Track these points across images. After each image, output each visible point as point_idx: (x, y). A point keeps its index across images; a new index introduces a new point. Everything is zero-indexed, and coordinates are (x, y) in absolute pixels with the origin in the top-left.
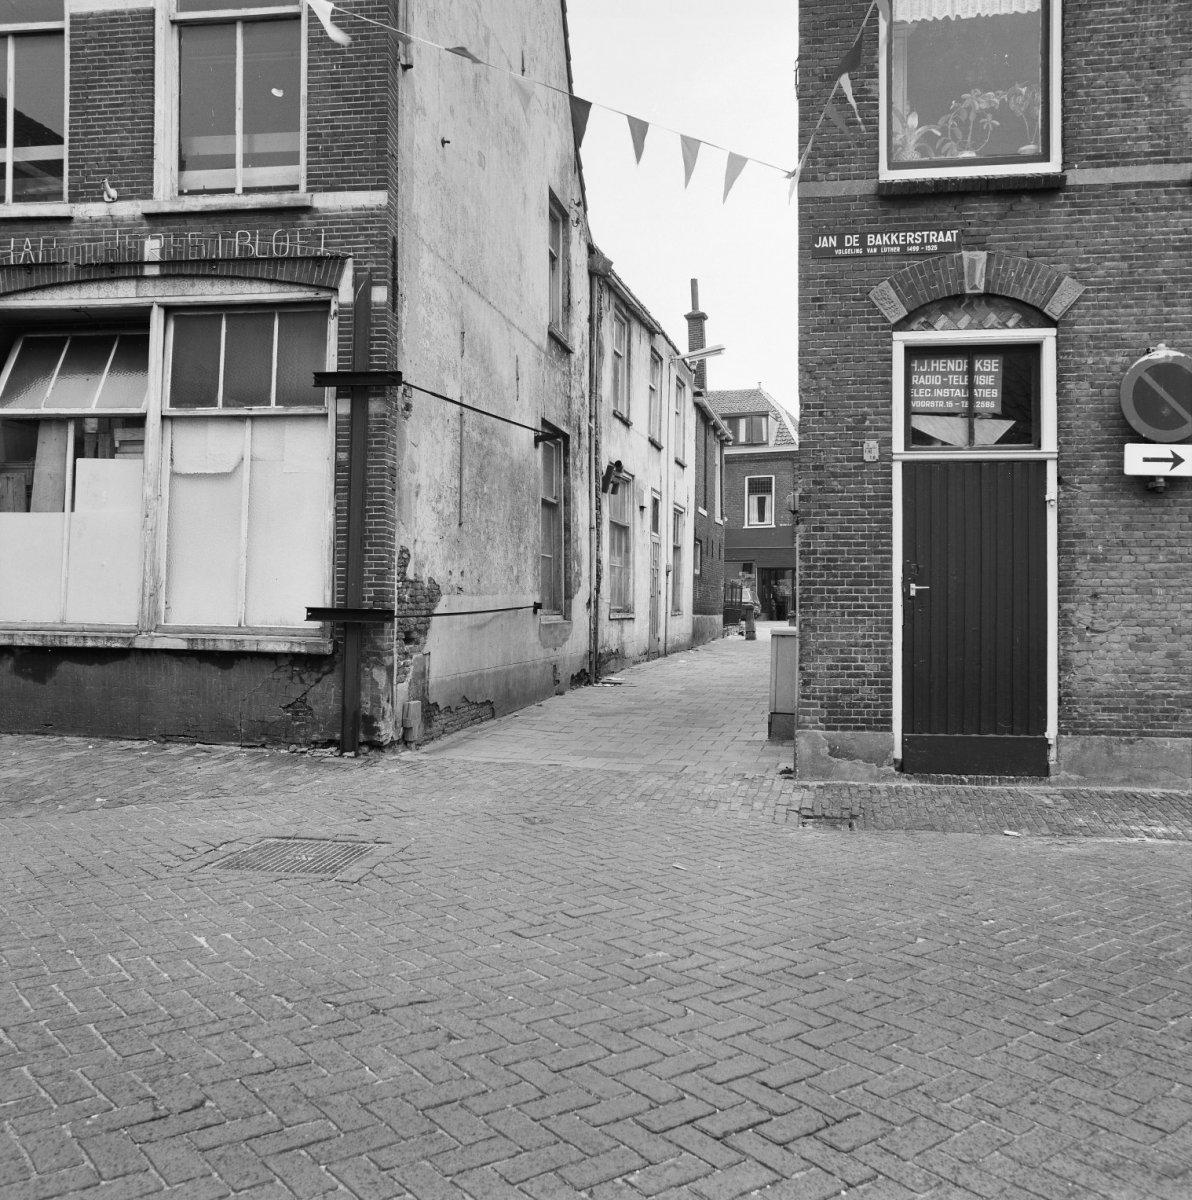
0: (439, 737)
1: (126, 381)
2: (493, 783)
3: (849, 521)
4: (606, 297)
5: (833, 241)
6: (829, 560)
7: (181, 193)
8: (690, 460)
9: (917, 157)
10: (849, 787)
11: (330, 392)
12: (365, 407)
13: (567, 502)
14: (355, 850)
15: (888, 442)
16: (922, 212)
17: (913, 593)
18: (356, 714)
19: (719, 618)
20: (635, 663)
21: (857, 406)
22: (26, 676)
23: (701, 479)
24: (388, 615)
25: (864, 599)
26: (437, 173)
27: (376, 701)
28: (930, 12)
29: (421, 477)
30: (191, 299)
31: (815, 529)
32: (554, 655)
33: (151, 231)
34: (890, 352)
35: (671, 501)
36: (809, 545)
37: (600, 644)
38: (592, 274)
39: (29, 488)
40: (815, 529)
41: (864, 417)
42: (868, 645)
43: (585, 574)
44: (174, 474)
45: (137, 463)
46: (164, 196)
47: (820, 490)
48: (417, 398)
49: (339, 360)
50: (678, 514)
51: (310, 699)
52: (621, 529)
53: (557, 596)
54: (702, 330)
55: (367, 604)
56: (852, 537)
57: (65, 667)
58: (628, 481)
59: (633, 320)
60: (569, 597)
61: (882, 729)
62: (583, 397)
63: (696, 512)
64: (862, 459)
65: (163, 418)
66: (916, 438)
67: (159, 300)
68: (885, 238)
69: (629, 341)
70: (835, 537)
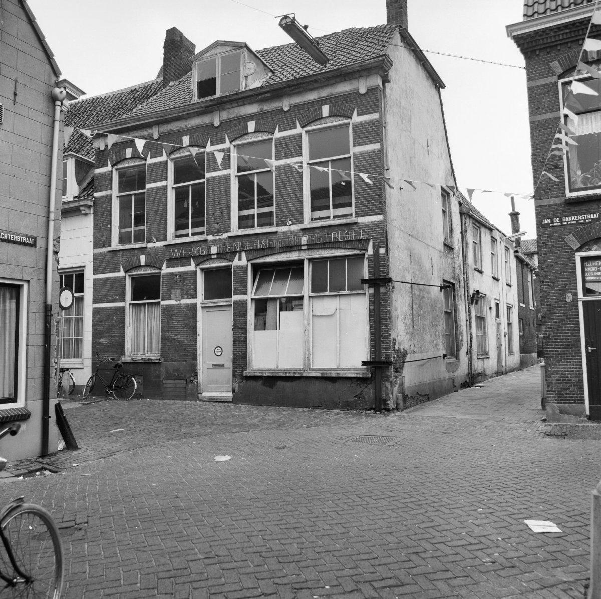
0: (408, 408)
1: (295, 283)
2: (431, 423)
3: (562, 324)
4: (468, 220)
5: (549, 221)
6: (555, 339)
7: (312, 220)
8: (514, 282)
9: (581, 186)
10: (567, 425)
11: (366, 286)
12: (379, 290)
13: (455, 311)
14: (389, 438)
15: (576, 294)
16: (584, 207)
17: (590, 351)
18: (380, 399)
19: (535, 355)
20: (491, 377)
21: (562, 281)
22: (267, 386)
23: (521, 291)
24: (390, 363)
25: (570, 354)
26: (399, 200)
27: (387, 394)
28: (583, 132)
29: (399, 312)
30: (317, 256)
31: (549, 328)
32: (453, 375)
33: (303, 234)
34: (575, 260)
35: (505, 303)
36: (546, 334)
37: (473, 369)
38: (461, 214)
39: (265, 321)
40: (549, 328)
41: (566, 285)
42: (573, 371)
43: (465, 340)
44: (313, 316)
45: (301, 312)
46: (307, 223)
47: (550, 313)
48: (396, 284)
49: (369, 274)
50: (509, 308)
51: (364, 393)
52: (481, 319)
53: (453, 350)
54: (518, 220)
55: (383, 359)
56: (564, 330)
57: (280, 384)
58: (483, 297)
59: (481, 227)
60: (458, 350)
61: (580, 403)
62: (460, 265)
63: (519, 306)
64: (566, 301)
65: (309, 297)
66: (587, 291)
67: (307, 257)
68: (570, 218)
69: (480, 236)
70: (557, 330)
